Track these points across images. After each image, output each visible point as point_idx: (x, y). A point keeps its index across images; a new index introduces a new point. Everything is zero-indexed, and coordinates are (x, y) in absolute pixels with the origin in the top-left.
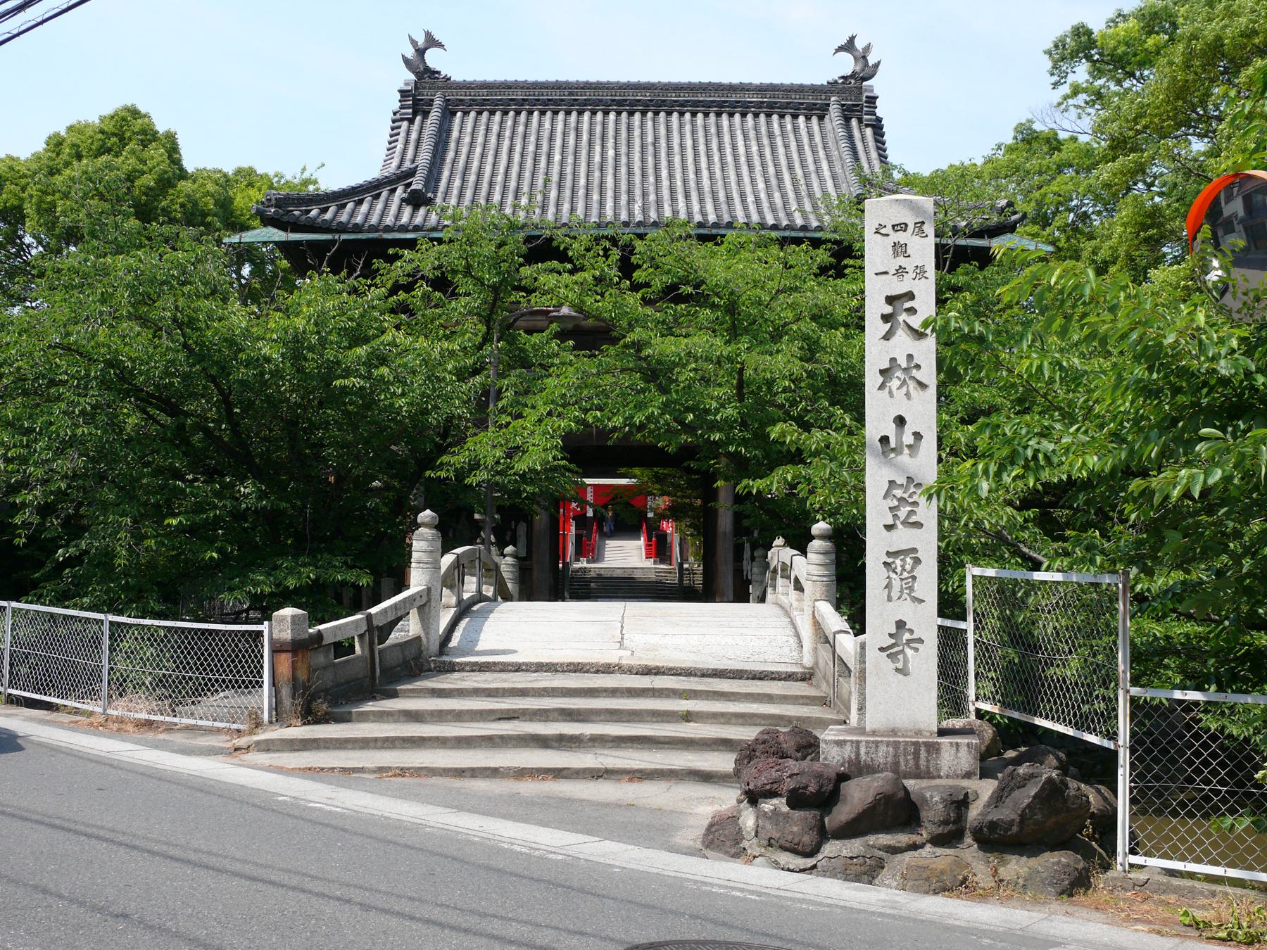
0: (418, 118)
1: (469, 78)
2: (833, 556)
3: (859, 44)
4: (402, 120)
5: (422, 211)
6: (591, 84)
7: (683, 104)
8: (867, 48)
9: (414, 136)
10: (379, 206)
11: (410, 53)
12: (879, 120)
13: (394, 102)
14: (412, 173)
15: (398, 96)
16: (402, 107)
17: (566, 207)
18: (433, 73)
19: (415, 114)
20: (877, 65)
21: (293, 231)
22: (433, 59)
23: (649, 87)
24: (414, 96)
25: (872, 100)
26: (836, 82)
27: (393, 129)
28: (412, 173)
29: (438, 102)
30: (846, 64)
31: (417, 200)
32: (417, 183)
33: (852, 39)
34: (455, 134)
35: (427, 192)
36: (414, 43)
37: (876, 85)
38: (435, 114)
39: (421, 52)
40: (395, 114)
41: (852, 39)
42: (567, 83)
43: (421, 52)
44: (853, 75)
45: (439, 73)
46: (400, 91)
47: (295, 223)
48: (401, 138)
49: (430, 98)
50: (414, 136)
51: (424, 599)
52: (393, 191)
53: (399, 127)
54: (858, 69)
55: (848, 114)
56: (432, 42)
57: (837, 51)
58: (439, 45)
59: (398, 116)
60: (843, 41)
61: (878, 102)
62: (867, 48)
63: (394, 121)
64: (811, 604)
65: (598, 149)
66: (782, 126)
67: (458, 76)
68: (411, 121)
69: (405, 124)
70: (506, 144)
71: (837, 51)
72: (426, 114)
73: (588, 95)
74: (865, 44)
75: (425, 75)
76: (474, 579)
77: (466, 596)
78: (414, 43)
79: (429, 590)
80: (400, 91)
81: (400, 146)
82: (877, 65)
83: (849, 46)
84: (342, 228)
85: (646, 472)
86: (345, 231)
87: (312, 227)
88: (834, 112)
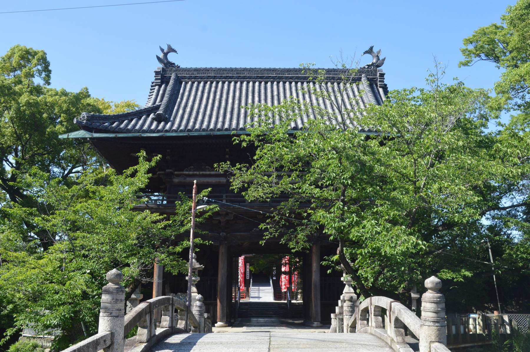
0: (163, 86)
1: (189, 67)
2: (443, 305)
3: (375, 50)
4: (156, 85)
5: (162, 124)
6: (252, 69)
7: (291, 78)
8: (379, 52)
9: (161, 92)
10: (141, 122)
11: (161, 55)
12: (386, 85)
13: (152, 78)
14: (158, 107)
15: (154, 74)
16: (156, 79)
17: (234, 122)
18: (172, 64)
19: (162, 83)
20: (384, 60)
21: (95, 132)
22: (171, 57)
23: (274, 70)
24: (162, 75)
25: (382, 75)
26: (364, 68)
27: (151, 90)
28: (158, 107)
29: (173, 76)
30: (370, 60)
31: (159, 119)
32: (160, 112)
33: (371, 48)
34: (181, 91)
35: (165, 115)
36: (162, 50)
37: (383, 69)
38: (171, 82)
39: (166, 55)
40: (153, 83)
41: (371, 48)
42: (236, 68)
43: (166, 55)
44: (373, 64)
45: (174, 64)
46: (156, 72)
47: (96, 128)
48: (154, 94)
49: (170, 77)
50: (161, 92)
51: (108, 343)
52: (148, 116)
53: (154, 89)
54: (374, 61)
55: (372, 83)
56: (171, 50)
57: (364, 53)
58: (174, 51)
59: (154, 84)
60: (367, 49)
61: (385, 76)
62: (379, 52)
63: (152, 86)
64: (427, 344)
65: (250, 97)
66: (339, 87)
67: (183, 65)
68: (160, 86)
69: (157, 87)
70: (206, 95)
71: (364, 53)
72: (167, 83)
73: (246, 74)
74: (378, 50)
75: (168, 65)
76: (168, 318)
77: (159, 331)
78: (162, 50)
79: (112, 334)
80: (156, 72)
81: (154, 97)
82: (384, 60)
83: (370, 51)
84: (121, 131)
85: (105, 114)
86: (122, 133)
87: (106, 131)
88: (364, 79)
